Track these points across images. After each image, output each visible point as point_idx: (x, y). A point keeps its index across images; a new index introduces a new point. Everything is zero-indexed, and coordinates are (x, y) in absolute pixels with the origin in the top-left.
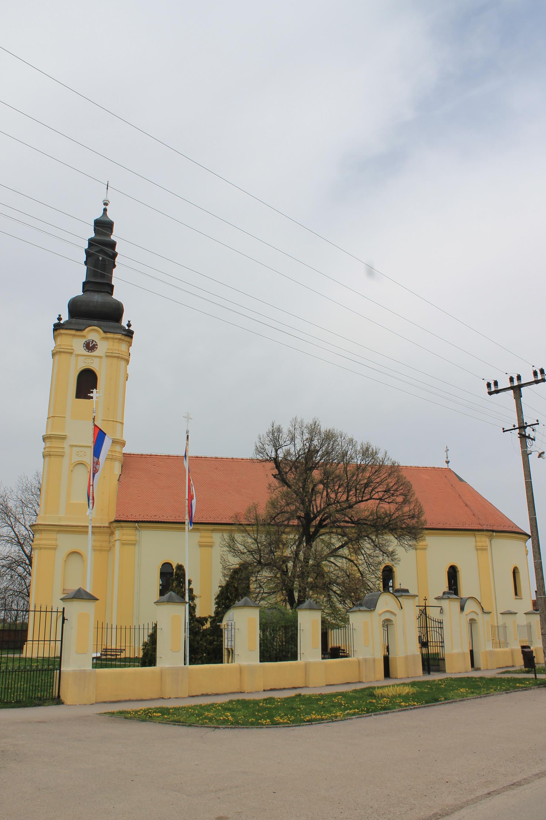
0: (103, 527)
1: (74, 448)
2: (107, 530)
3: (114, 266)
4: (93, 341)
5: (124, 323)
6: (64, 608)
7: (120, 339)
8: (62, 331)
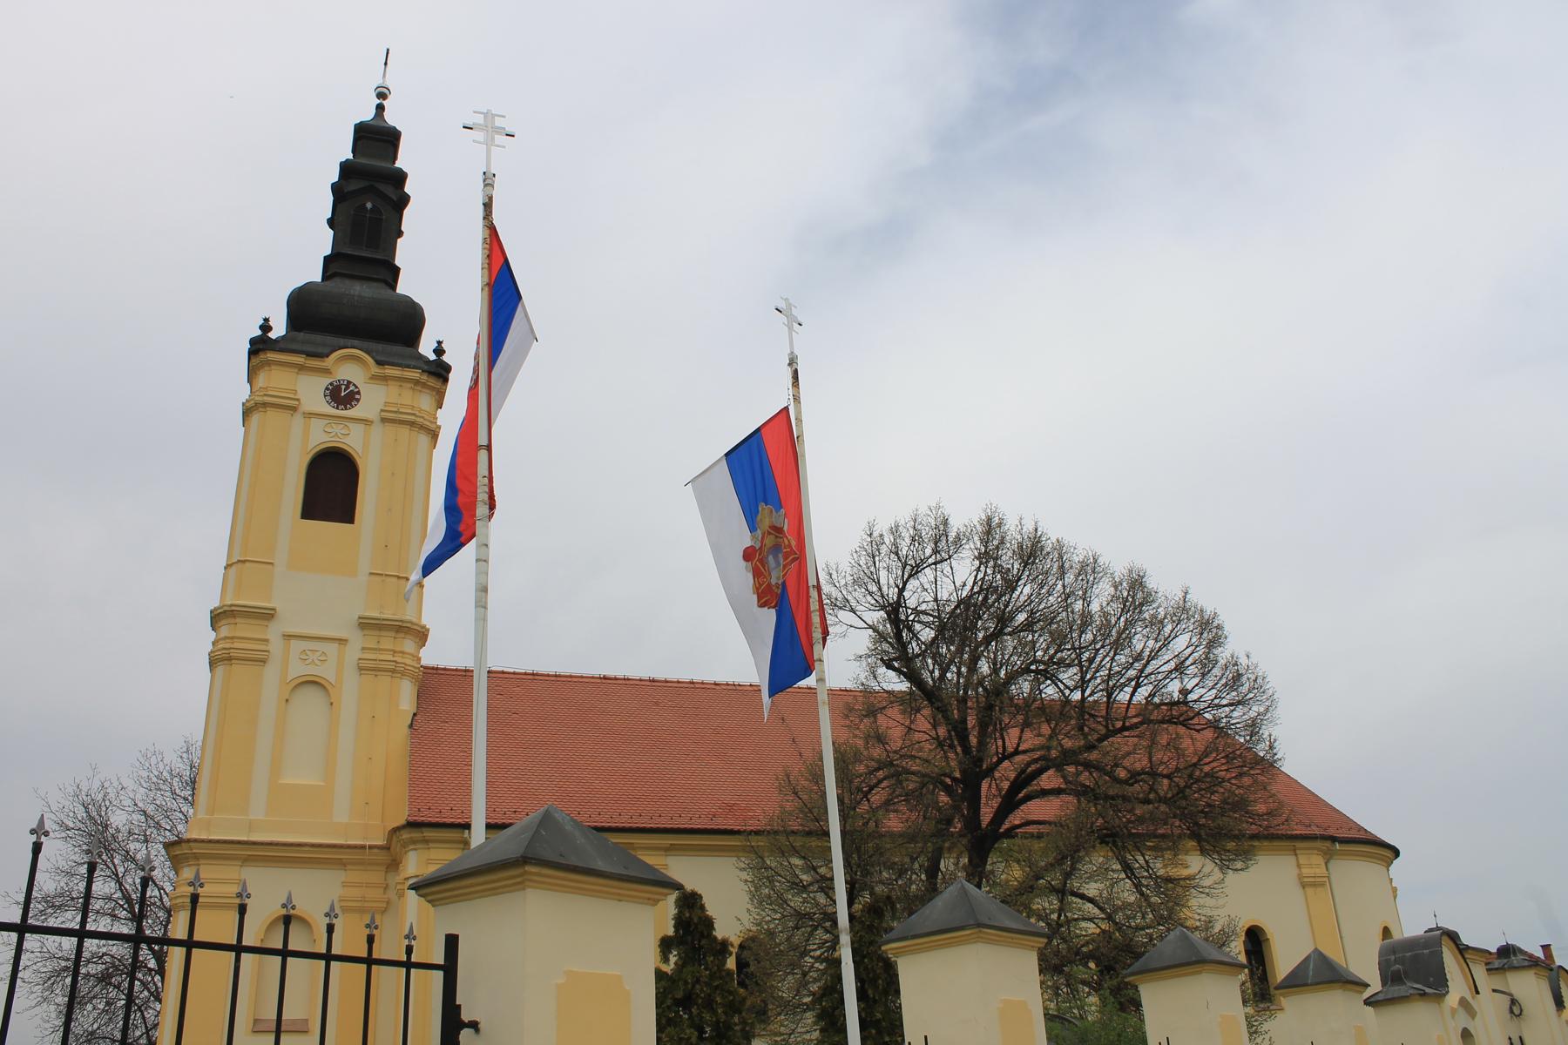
0: (371, 847)
1: (293, 642)
2: (382, 856)
5: (426, 348)
6: (452, 942)
7: (417, 382)
8: (271, 356)
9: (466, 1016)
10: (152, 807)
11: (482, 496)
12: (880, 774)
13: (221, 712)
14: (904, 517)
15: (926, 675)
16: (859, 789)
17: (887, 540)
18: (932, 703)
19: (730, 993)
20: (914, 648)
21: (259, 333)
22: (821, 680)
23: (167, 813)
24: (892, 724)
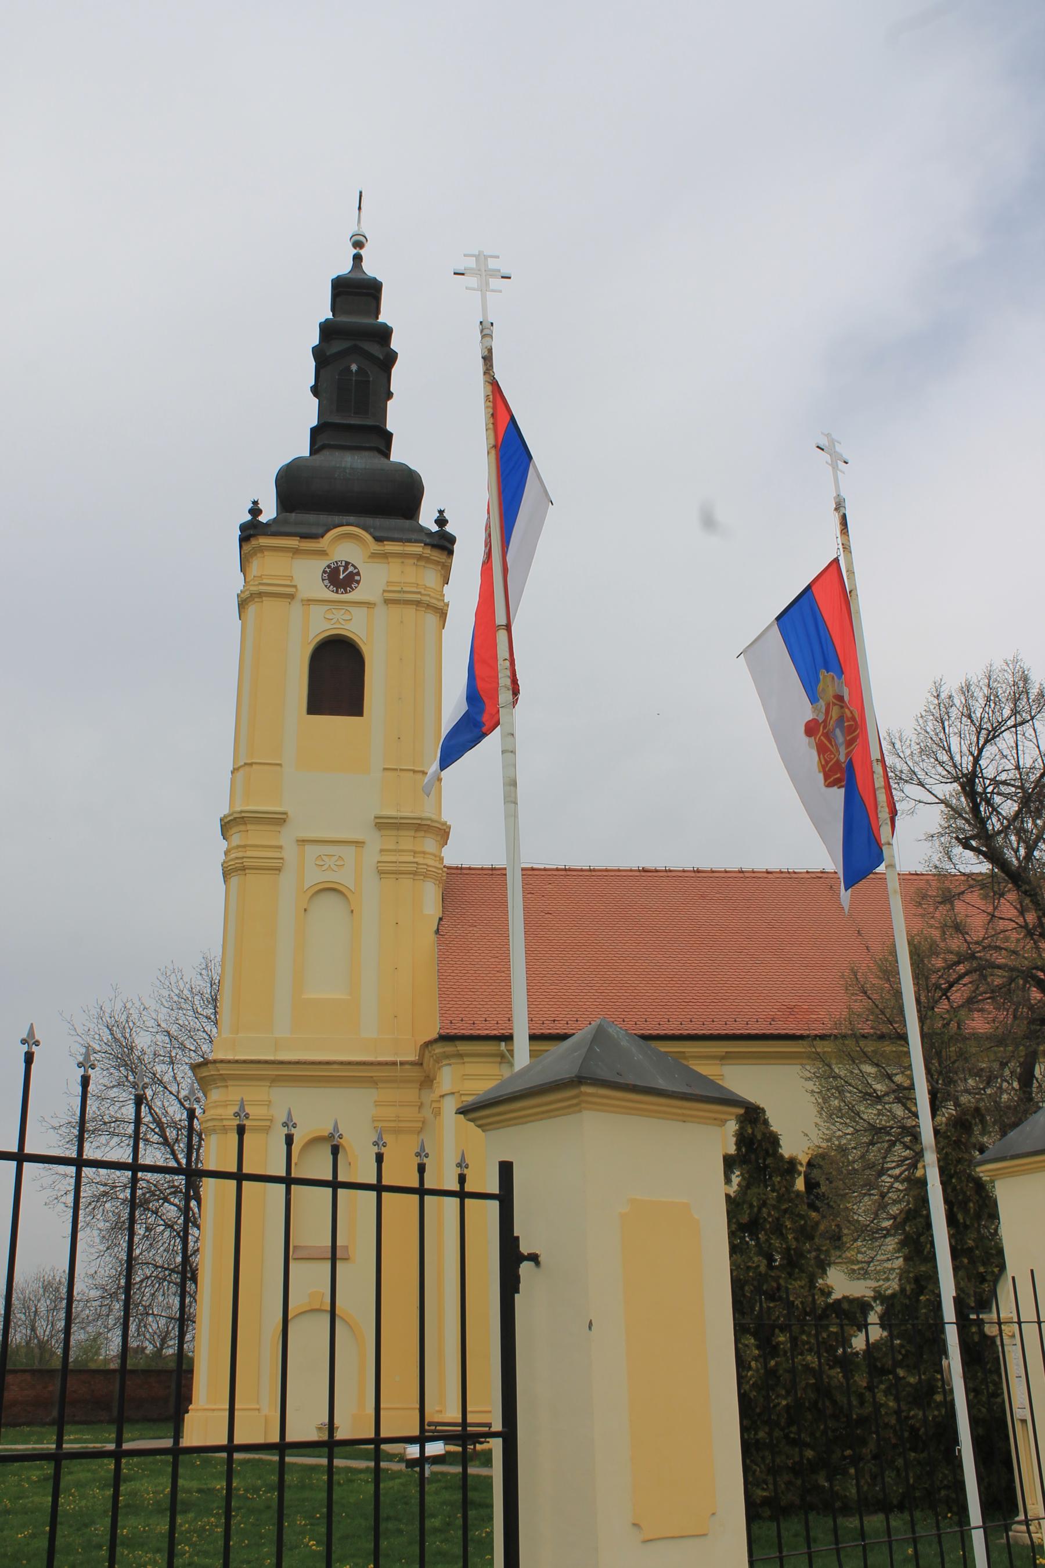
0: (402, 1063)
1: (309, 849)
2: (415, 1073)
3: (389, 395)
4: (347, 563)
5: (427, 519)
6: (506, 1170)
7: (420, 557)
8: (263, 541)
9: (524, 1249)
10: (175, 1027)
11: (504, 681)
12: (961, 968)
13: (239, 922)
14: (976, 674)
15: (1009, 854)
16: (937, 987)
17: (957, 702)
18: (1018, 887)
19: (802, 1217)
20: (994, 824)
21: (249, 517)
22: (891, 866)
23: (190, 1033)
24: (973, 911)
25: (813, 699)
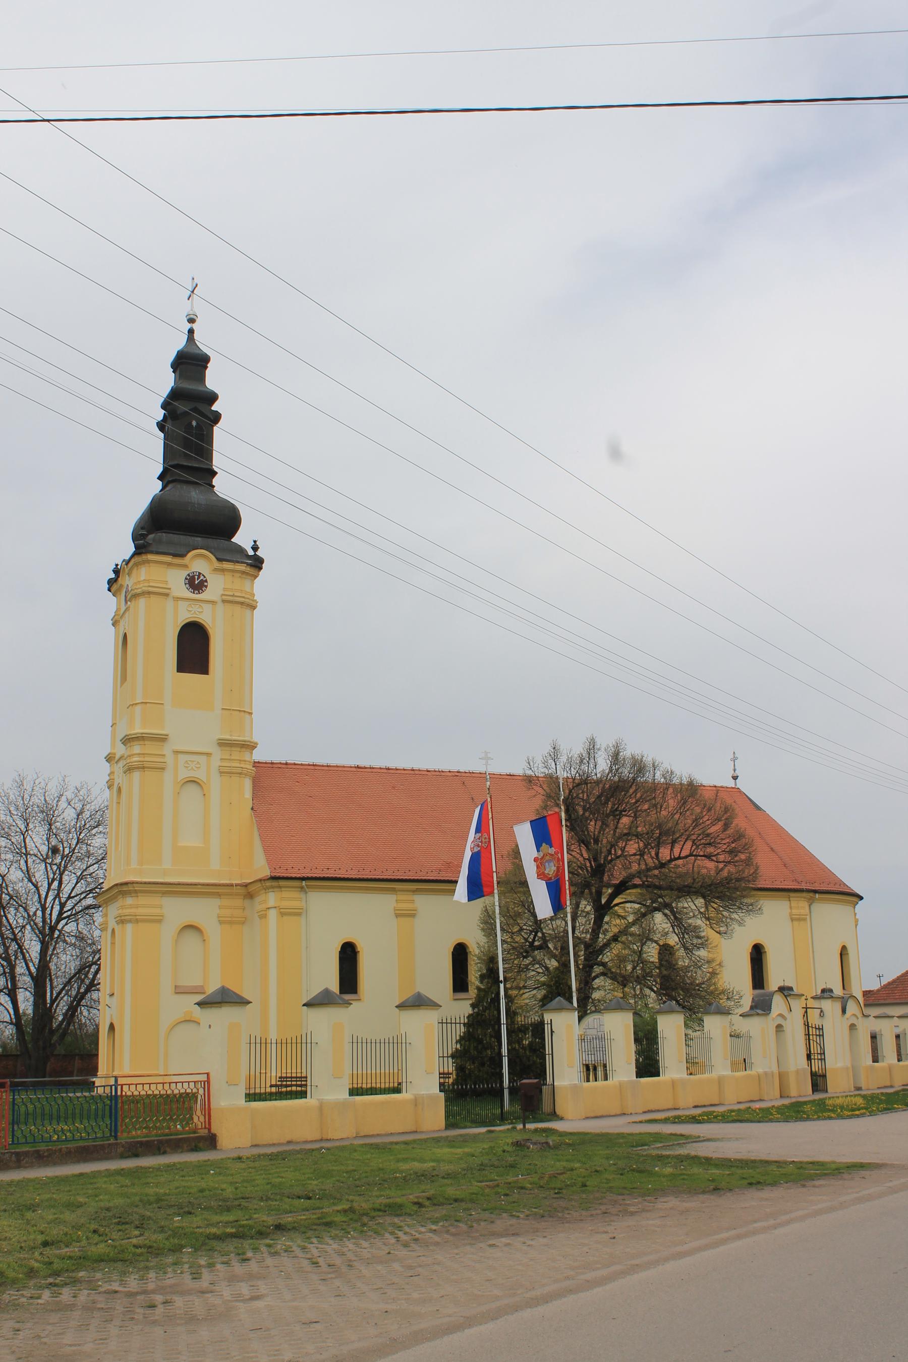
1: (180, 756)
4: (200, 573)
7: (243, 573)
25: (538, 851)
